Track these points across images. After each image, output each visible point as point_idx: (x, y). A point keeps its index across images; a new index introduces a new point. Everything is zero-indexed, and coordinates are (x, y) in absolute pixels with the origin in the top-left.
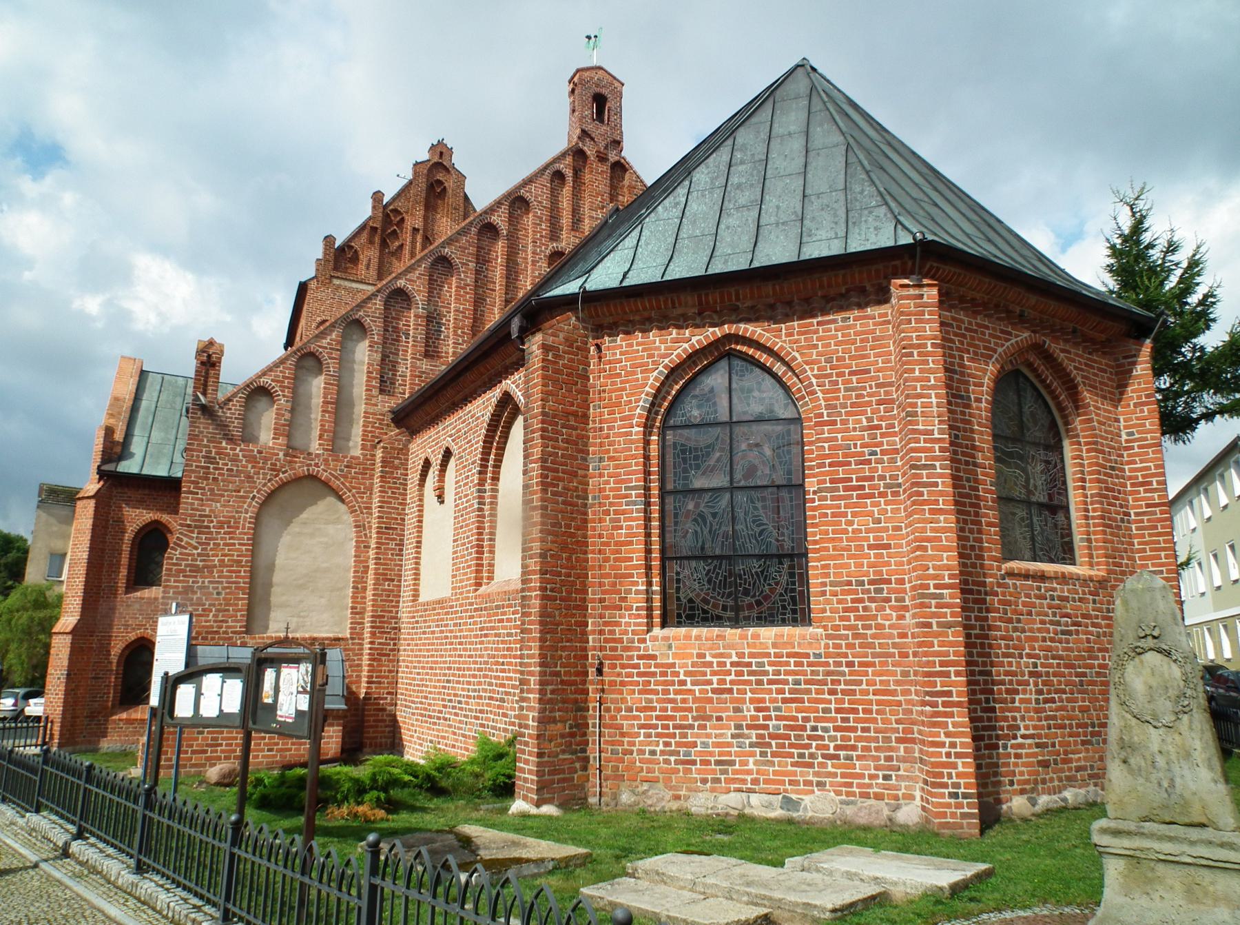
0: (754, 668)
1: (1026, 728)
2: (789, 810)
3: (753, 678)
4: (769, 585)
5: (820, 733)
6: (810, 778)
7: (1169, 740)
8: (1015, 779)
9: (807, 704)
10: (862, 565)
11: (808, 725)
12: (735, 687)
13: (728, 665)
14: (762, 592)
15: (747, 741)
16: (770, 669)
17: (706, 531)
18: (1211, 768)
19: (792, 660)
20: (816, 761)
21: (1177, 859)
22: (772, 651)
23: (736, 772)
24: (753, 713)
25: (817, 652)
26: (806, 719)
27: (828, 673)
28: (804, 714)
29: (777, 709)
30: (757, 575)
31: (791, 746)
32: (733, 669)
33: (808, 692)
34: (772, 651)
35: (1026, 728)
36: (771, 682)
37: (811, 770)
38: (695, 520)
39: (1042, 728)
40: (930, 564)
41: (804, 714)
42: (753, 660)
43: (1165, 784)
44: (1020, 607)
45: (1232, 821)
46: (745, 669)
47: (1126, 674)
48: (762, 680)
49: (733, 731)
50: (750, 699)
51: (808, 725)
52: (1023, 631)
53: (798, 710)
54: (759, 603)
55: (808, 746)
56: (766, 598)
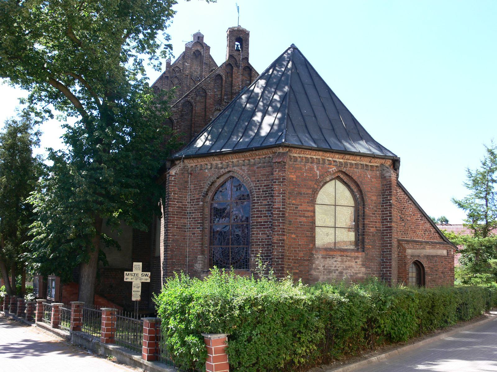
17: (222, 238)
38: (219, 234)
54: (236, 262)
56: (239, 260)
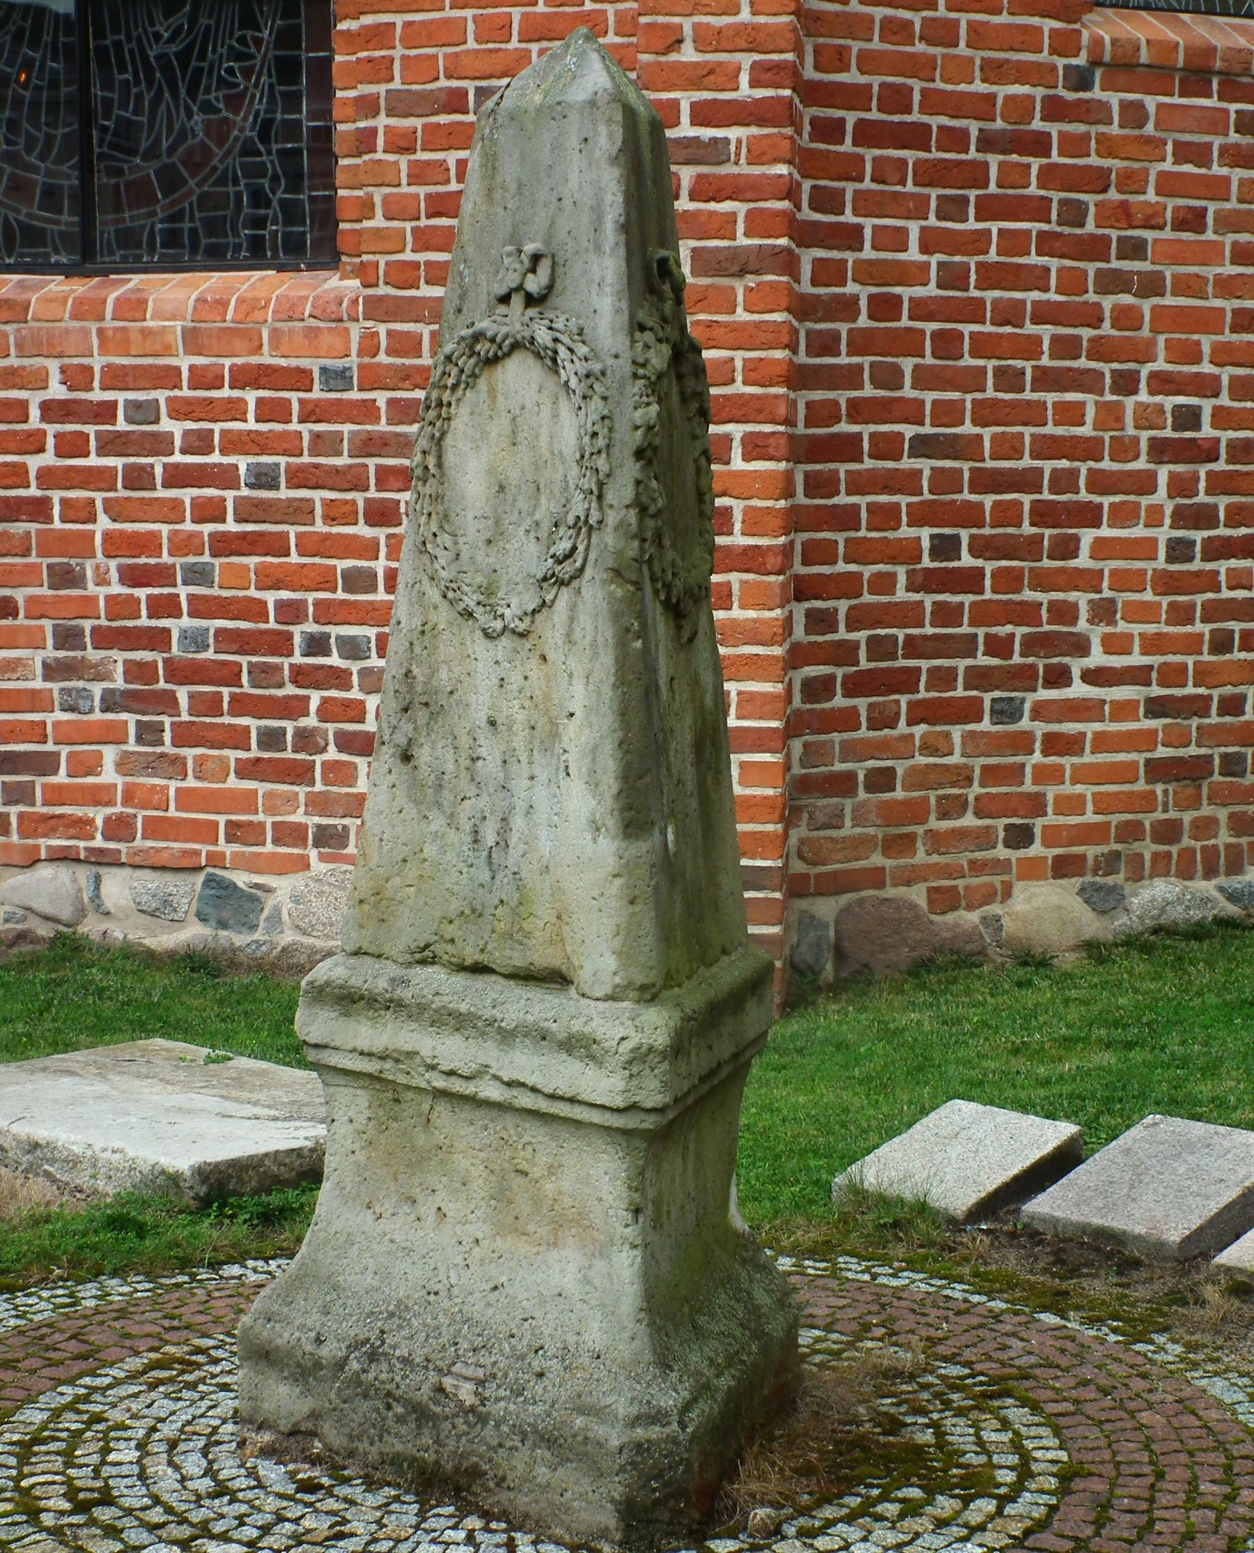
0: (121, 425)
1: (1114, 645)
2: (223, 925)
3: (117, 462)
4: (208, 108)
5: (334, 660)
6: (298, 817)
7: (515, 680)
8: (1039, 824)
9: (294, 558)
10: (504, 29)
11: (298, 633)
12: (56, 496)
13: (35, 413)
14: (183, 135)
15: (97, 689)
16: (175, 428)
18: (593, 783)
19: (251, 397)
20: (319, 759)
21: (469, 1088)
22: (184, 363)
23: (56, 795)
24: (117, 589)
25: (339, 363)
26: (293, 613)
27: (369, 445)
28: (285, 595)
29: (198, 575)
30: (167, 68)
31: (241, 705)
32: (51, 429)
33: (301, 512)
34: (184, 363)
35: (1114, 645)
36: (177, 477)
37: (302, 791)
39: (1192, 644)
40: (687, 25)
41: (285, 595)
42: (121, 397)
43: (490, 838)
44: (1151, 196)
45: (611, 962)
46: (90, 430)
47: (448, 440)
48: (148, 471)
49: (51, 653)
50: (107, 536)
51: (298, 633)
52: (1151, 286)
53: (270, 580)
55: (296, 708)
56: (198, 160)
